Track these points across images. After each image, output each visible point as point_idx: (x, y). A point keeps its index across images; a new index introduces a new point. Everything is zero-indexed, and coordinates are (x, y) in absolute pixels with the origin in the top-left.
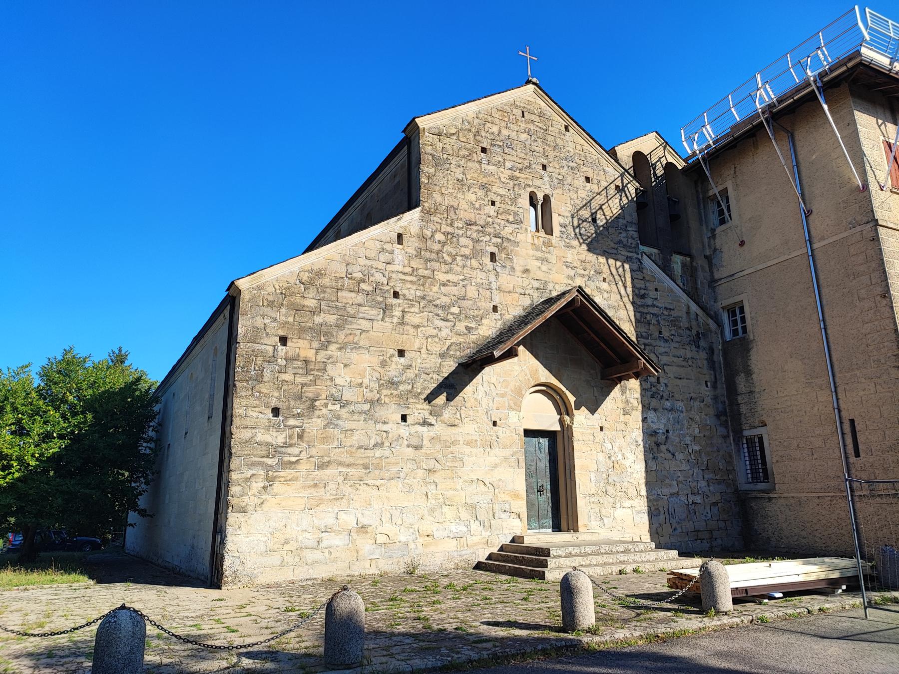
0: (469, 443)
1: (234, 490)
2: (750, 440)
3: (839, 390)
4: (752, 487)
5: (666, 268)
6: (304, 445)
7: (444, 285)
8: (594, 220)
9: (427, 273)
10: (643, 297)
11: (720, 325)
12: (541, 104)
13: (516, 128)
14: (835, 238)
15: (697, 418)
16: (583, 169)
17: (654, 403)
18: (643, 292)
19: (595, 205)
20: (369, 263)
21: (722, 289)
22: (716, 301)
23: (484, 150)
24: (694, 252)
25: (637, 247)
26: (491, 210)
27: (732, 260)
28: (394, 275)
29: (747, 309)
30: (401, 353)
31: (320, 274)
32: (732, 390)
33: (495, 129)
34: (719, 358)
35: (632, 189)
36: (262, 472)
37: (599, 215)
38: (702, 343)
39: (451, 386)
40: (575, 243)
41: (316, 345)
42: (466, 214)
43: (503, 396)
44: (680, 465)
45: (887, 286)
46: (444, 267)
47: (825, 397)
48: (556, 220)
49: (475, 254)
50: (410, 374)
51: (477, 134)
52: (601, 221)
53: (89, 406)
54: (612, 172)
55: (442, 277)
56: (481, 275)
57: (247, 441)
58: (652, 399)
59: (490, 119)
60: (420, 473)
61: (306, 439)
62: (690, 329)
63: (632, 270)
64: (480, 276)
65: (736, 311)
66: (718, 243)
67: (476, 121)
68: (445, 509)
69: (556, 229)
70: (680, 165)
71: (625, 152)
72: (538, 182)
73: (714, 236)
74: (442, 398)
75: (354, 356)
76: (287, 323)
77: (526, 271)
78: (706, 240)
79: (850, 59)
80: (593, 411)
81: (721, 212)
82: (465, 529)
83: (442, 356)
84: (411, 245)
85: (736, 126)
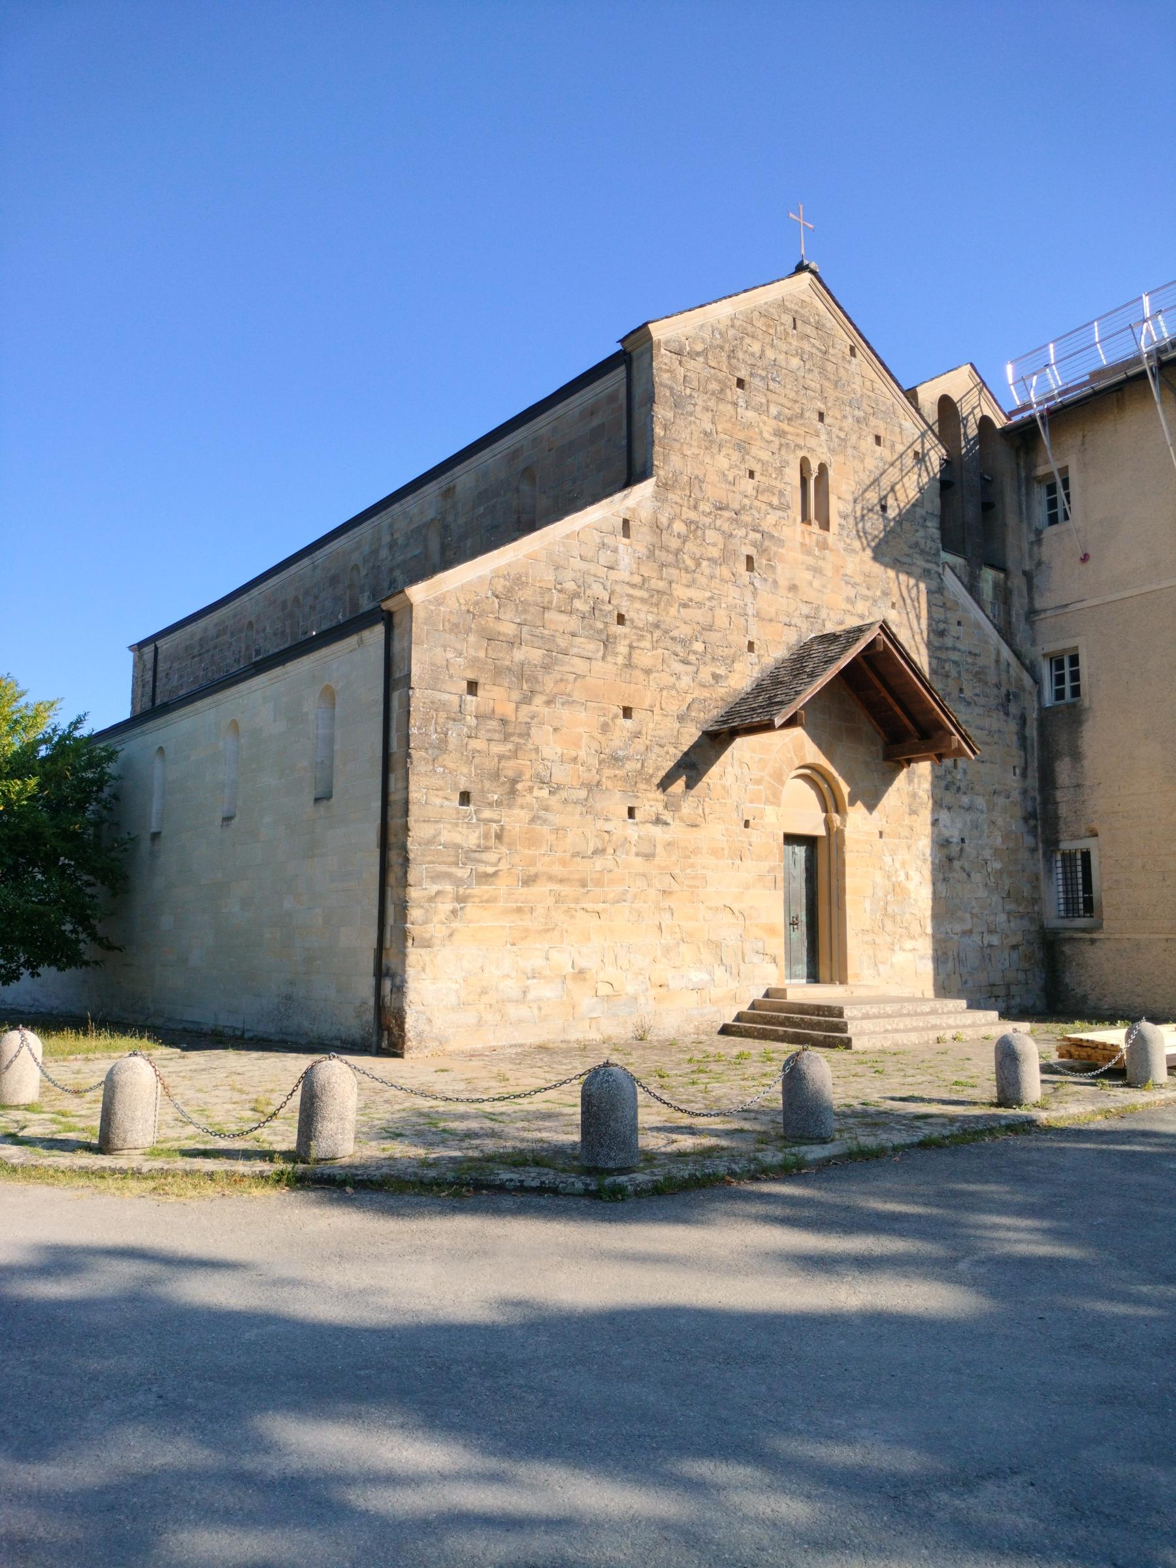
0: (716, 852)
1: (415, 914)
2: (1068, 858)
4: (1066, 923)
5: (973, 589)
6: (504, 849)
7: (685, 606)
8: (884, 508)
9: (661, 585)
11: (1037, 681)
12: (820, 306)
13: (784, 347)
15: (1000, 822)
16: (873, 421)
17: (949, 798)
18: (942, 626)
19: (885, 482)
20: (584, 566)
21: (1044, 625)
22: (1034, 642)
23: (740, 383)
24: (1011, 565)
25: (937, 554)
26: (748, 485)
27: (1064, 582)
28: (618, 588)
29: (1083, 660)
30: (627, 712)
31: (518, 581)
32: (1047, 781)
34: (1032, 732)
35: (936, 456)
36: (449, 888)
37: (890, 501)
39: (692, 766)
40: (857, 544)
41: (516, 695)
42: (715, 491)
43: (758, 782)
46: (686, 578)
49: (727, 556)
50: (639, 744)
51: (732, 355)
52: (892, 513)
55: (681, 592)
57: (430, 842)
59: (750, 329)
60: (652, 893)
61: (506, 839)
63: (929, 592)
64: (732, 594)
65: (1066, 665)
66: (1045, 552)
67: (731, 332)
68: (683, 948)
70: (999, 422)
71: (929, 395)
73: (1039, 541)
74: (680, 784)
75: (565, 713)
76: (476, 659)
77: (793, 588)
80: (871, 807)
81: (1052, 504)
82: (706, 977)
83: (681, 718)
85: (1097, 375)
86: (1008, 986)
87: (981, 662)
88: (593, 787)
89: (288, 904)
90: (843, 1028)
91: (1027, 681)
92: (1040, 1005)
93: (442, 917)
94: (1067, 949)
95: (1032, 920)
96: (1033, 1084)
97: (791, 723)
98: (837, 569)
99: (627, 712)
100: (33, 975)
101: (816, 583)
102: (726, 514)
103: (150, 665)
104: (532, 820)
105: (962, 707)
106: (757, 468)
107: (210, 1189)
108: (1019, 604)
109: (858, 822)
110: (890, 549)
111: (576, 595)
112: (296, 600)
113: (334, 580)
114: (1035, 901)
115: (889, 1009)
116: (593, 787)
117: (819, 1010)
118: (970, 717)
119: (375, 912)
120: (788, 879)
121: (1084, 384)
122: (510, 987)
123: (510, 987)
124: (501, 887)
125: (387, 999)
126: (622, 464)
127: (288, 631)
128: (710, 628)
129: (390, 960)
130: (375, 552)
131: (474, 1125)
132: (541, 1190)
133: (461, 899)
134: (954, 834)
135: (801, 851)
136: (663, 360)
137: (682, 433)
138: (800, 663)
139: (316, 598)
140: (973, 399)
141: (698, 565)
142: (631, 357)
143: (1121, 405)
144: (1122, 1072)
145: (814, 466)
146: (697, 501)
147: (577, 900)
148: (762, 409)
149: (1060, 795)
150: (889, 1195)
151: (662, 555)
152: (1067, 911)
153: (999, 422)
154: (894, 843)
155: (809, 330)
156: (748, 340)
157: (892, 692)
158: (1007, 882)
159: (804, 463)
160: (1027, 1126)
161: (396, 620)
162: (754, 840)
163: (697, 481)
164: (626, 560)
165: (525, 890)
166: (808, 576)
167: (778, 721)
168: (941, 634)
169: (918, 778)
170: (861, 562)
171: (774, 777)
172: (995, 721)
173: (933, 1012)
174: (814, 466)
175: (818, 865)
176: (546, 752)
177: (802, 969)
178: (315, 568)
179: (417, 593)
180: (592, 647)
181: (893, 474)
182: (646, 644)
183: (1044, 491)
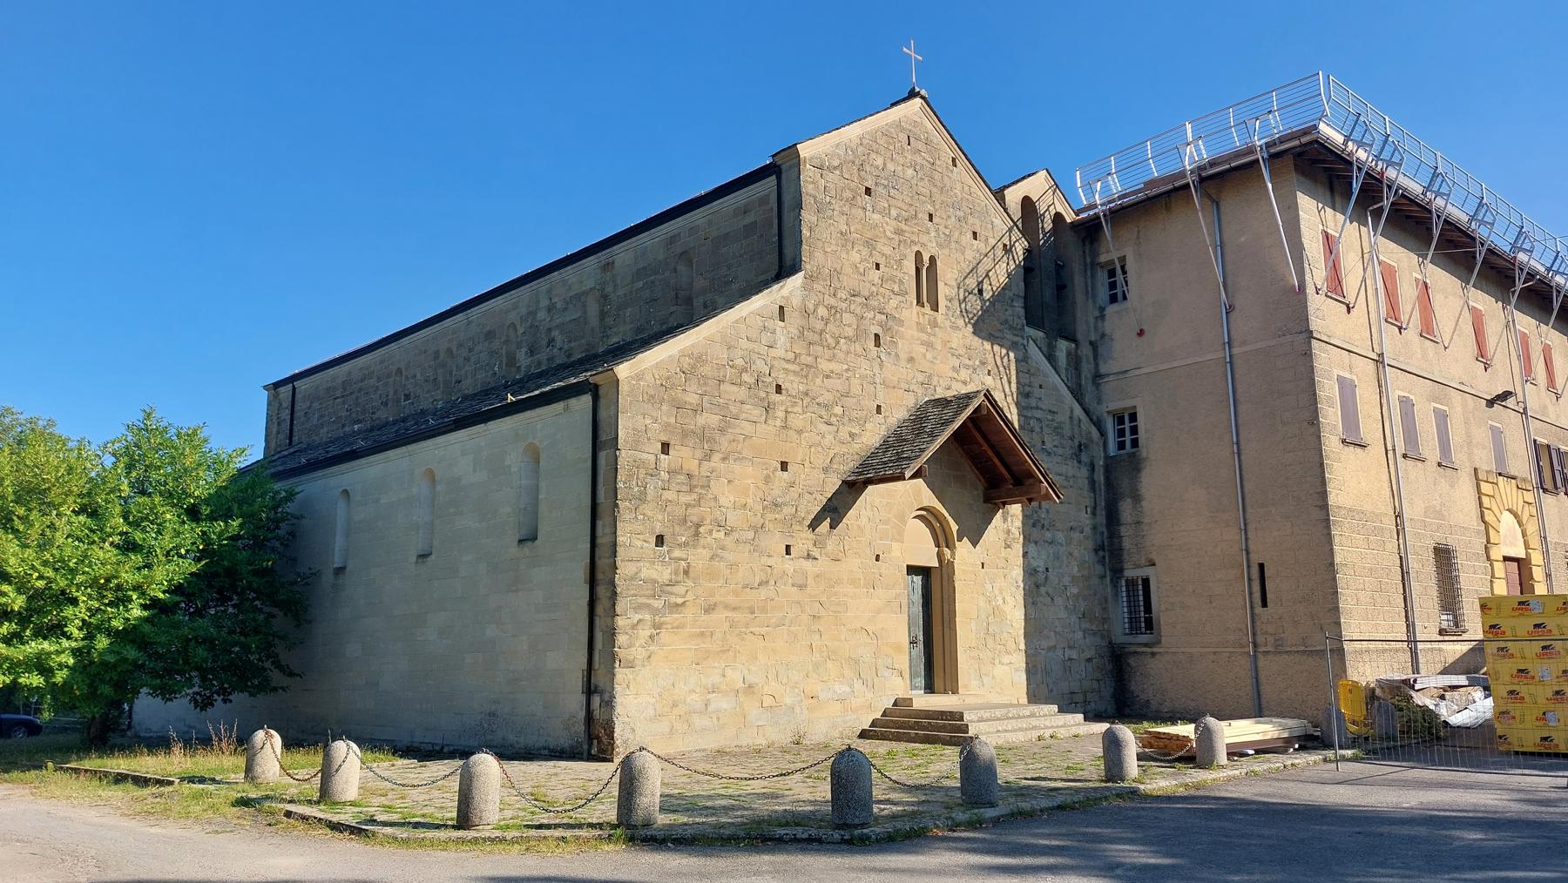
0: (854, 582)
1: (621, 639)
2: (1131, 583)
3: (1250, 527)
4: (1130, 639)
5: (1051, 358)
6: (690, 583)
7: (828, 377)
8: (981, 292)
9: (810, 360)
10: (1027, 395)
11: (1103, 434)
12: (929, 125)
13: (901, 161)
14: (1259, 345)
15: (1076, 553)
16: (971, 220)
17: (1036, 533)
18: (1027, 389)
19: (981, 270)
20: (750, 345)
21: (1109, 386)
22: (1099, 401)
23: (868, 191)
24: (1079, 337)
25: (1022, 329)
26: (875, 275)
27: (1123, 352)
28: (776, 363)
29: (1140, 418)
30: (784, 466)
31: (700, 359)
32: (1113, 517)
33: (880, 162)
34: (1100, 477)
35: (1020, 248)
36: (648, 617)
37: (986, 286)
38: (1084, 458)
39: (834, 510)
40: (961, 322)
41: (699, 454)
42: (849, 281)
43: (886, 522)
44: (1058, 613)
45: (1316, 410)
46: (828, 353)
47: (1232, 534)
48: (943, 291)
49: (858, 336)
50: (794, 493)
51: (861, 168)
52: (987, 295)
53: (221, 505)
54: (1000, 224)
55: (825, 366)
56: (865, 364)
57: (632, 579)
58: (1032, 525)
59: (875, 146)
60: (805, 617)
61: (692, 574)
62: (1072, 438)
63: (1017, 361)
64: (864, 366)
65: (1127, 421)
66: (1108, 326)
67: (860, 149)
68: (830, 664)
69: (942, 303)
70: (1069, 217)
71: (1014, 196)
72: (924, 238)
73: (1102, 317)
74: (826, 523)
75: (737, 468)
76: (668, 424)
77: (911, 360)
78: (1092, 320)
79: (1305, 132)
80: (975, 544)
81: (1113, 286)
82: (848, 689)
83: (825, 470)
84: (793, 318)
85: (1150, 184)
86: (1085, 693)
87: (1058, 418)
88: (758, 529)
89: (491, 631)
90: (965, 729)
91: (1094, 430)
92: (1111, 709)
93: (642, 641)
94: (1132, 661)
95: (1103, 637)
96: (1132, 767)
97: (913, 477)
98: (945, 343)
99: (784, 466)
100: (225, 701)
101: (929, 356)
102: (858, 299)
103: (286, 404)
104: (712, 558)
105: (1044, 457)
106: (882, 261)
107: (572, 848)
108: (1087, 369)
109: (964, 554)
110: (987, 325)
111: (745, 370)
112: (449, 351)
113: (490, 335)
114: (1105, 620)
115: (998, 713)
116: (758, 529)
117: (942, 715)
118: (1054, 467)
119: (585, 639)
120: (911, 603)
121: (1140, 191)
122: (695, 700)
123: (695, 700)
124: (689, 614)
125: (596, 713)
126: (774, 258)
127: (440, 378)
128: (847, 395)
129: (599, 679)
130: (533, 313)
131: (724, 802)
132: (810, 840)
133: (657, 626)
134: (1040, 564)
135: (918, 580)
136: (808, 172)
137: (823, 233)
138: (919, 423)
139: (471, 350)
140: (1049, 198)
141: (838, 343)
142: (780, 171)
143: (1168, 208)
144: (1195, 756)
145: (926, 259)
146: (836, 290)
147: (747, 625)
148: (885, 213)
149: (1124, 531)
150: (1049, 836)
151: (810, 336)
152: (1131, 628)
153: (1069, 217)
154: (994, 573)
155: (920, 146)
156: (873, 156)
157: (992, 447)
158: (1082, 606)
159: (918, 255)
160: (1133, 793)
161: (602, 392)
162: (883, 571)
163: (836, 273)
164: (782, 340)
165: (705, 617)
166: (922, 349)
167: (908, 474)
168: (1027, 395)
169: (1010, 520)
170: (964, 336)
171: (898, 516)
172: (1070, 468)
173: (1032, 715)
174: (926, 259)
175: (933, 590)
176: (722, 501)
177: (921, 681)
178: (469, 323)
179: (623, 370)
180: (757, 413)
181: (987, 263)
182: (798, 409)
183: (1106, 275)
